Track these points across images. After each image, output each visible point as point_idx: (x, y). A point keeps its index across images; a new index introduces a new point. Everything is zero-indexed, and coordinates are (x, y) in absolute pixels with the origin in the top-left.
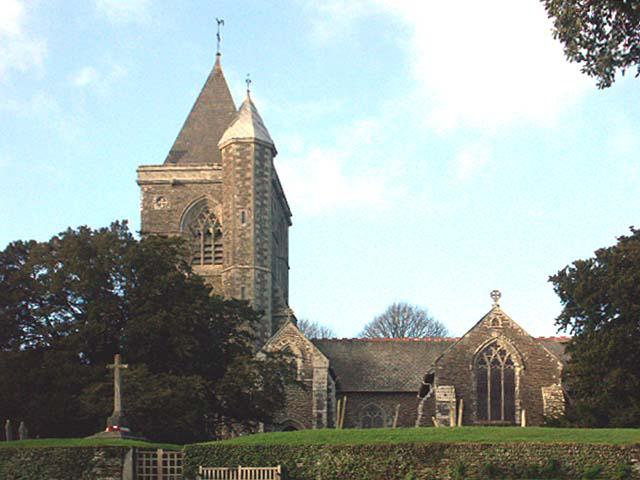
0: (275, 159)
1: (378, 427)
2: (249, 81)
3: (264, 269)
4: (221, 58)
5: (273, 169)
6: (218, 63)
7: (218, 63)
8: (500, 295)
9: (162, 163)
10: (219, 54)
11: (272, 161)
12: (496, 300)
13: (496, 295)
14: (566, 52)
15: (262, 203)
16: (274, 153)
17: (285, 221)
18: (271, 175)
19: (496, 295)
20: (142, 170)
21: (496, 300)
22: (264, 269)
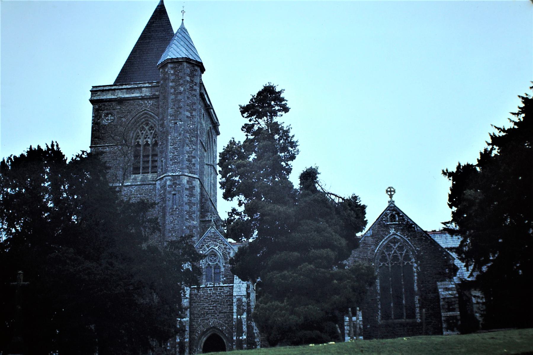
0: (203, 75)
1: (434, 333)
2: (183, 12)
3: (192, 175)
4: (184, 21)
5: (202, 85)
6: (183, 23)
7: (183, 23)
8: (394, 191)
9: (112, 83)
10: (183, 20)
11: (201, 76)
12: (391, 196)
13: (391, 192)
14: (450, 188)
15: (191, 113)
16: (203, 70)
17: (213, 131)
18: (200, 89)
19: (391, 192)
20: (95, 91)
21: (391, 196)
22: (192, 175)
